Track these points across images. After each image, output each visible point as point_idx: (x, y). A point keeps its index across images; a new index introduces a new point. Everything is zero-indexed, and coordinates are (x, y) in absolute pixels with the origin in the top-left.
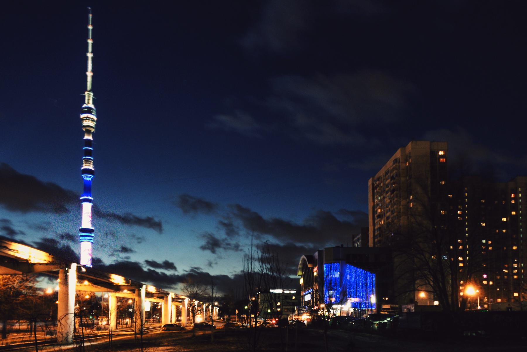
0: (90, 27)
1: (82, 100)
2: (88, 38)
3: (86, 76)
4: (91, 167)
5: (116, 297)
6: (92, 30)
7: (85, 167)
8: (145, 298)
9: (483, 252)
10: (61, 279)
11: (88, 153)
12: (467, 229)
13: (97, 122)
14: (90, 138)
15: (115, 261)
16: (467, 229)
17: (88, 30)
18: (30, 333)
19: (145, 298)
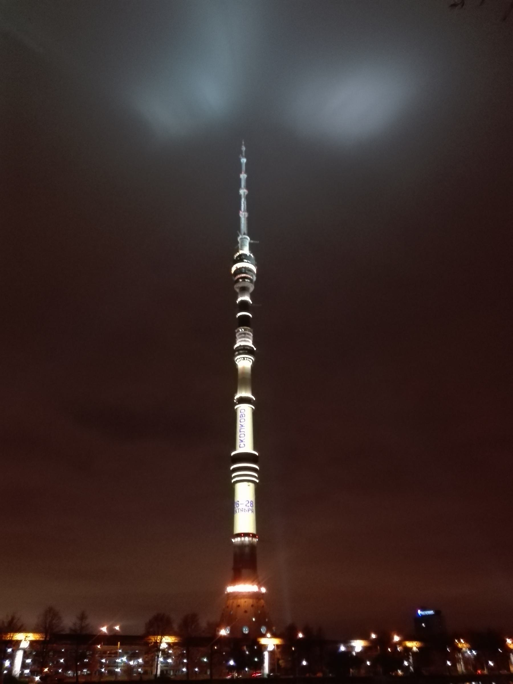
0: (244, 160)
1: (235, 246)
2: (241, 173)
3: (239, 219)
4: (249, 343)
5: (22, 640)
6: (247, 164)
7: (239, 343)
8: (355, 647)
9: (247, 653)
10: (249, 541)
11: (244, 321)
12: (423, 625)
13: (257, 275)
14: (246, 298)
15: (18, 619)
16: (423, 625)
17: (240, 164)
18: (79, 680)
19: (355, 647)
